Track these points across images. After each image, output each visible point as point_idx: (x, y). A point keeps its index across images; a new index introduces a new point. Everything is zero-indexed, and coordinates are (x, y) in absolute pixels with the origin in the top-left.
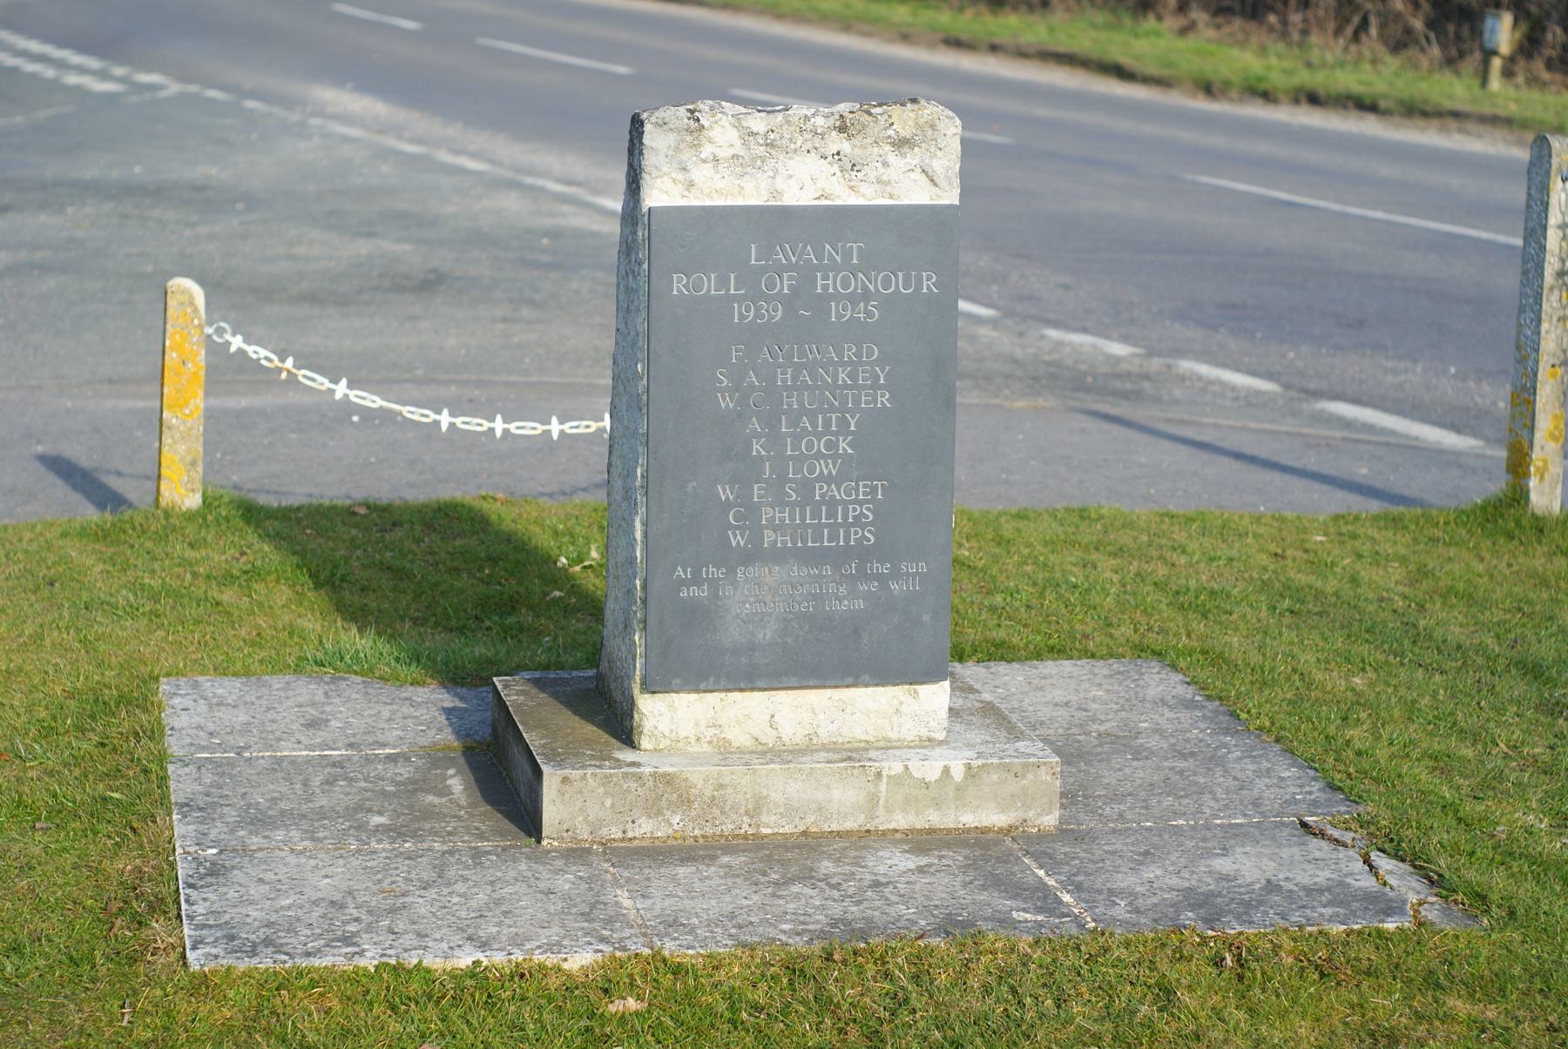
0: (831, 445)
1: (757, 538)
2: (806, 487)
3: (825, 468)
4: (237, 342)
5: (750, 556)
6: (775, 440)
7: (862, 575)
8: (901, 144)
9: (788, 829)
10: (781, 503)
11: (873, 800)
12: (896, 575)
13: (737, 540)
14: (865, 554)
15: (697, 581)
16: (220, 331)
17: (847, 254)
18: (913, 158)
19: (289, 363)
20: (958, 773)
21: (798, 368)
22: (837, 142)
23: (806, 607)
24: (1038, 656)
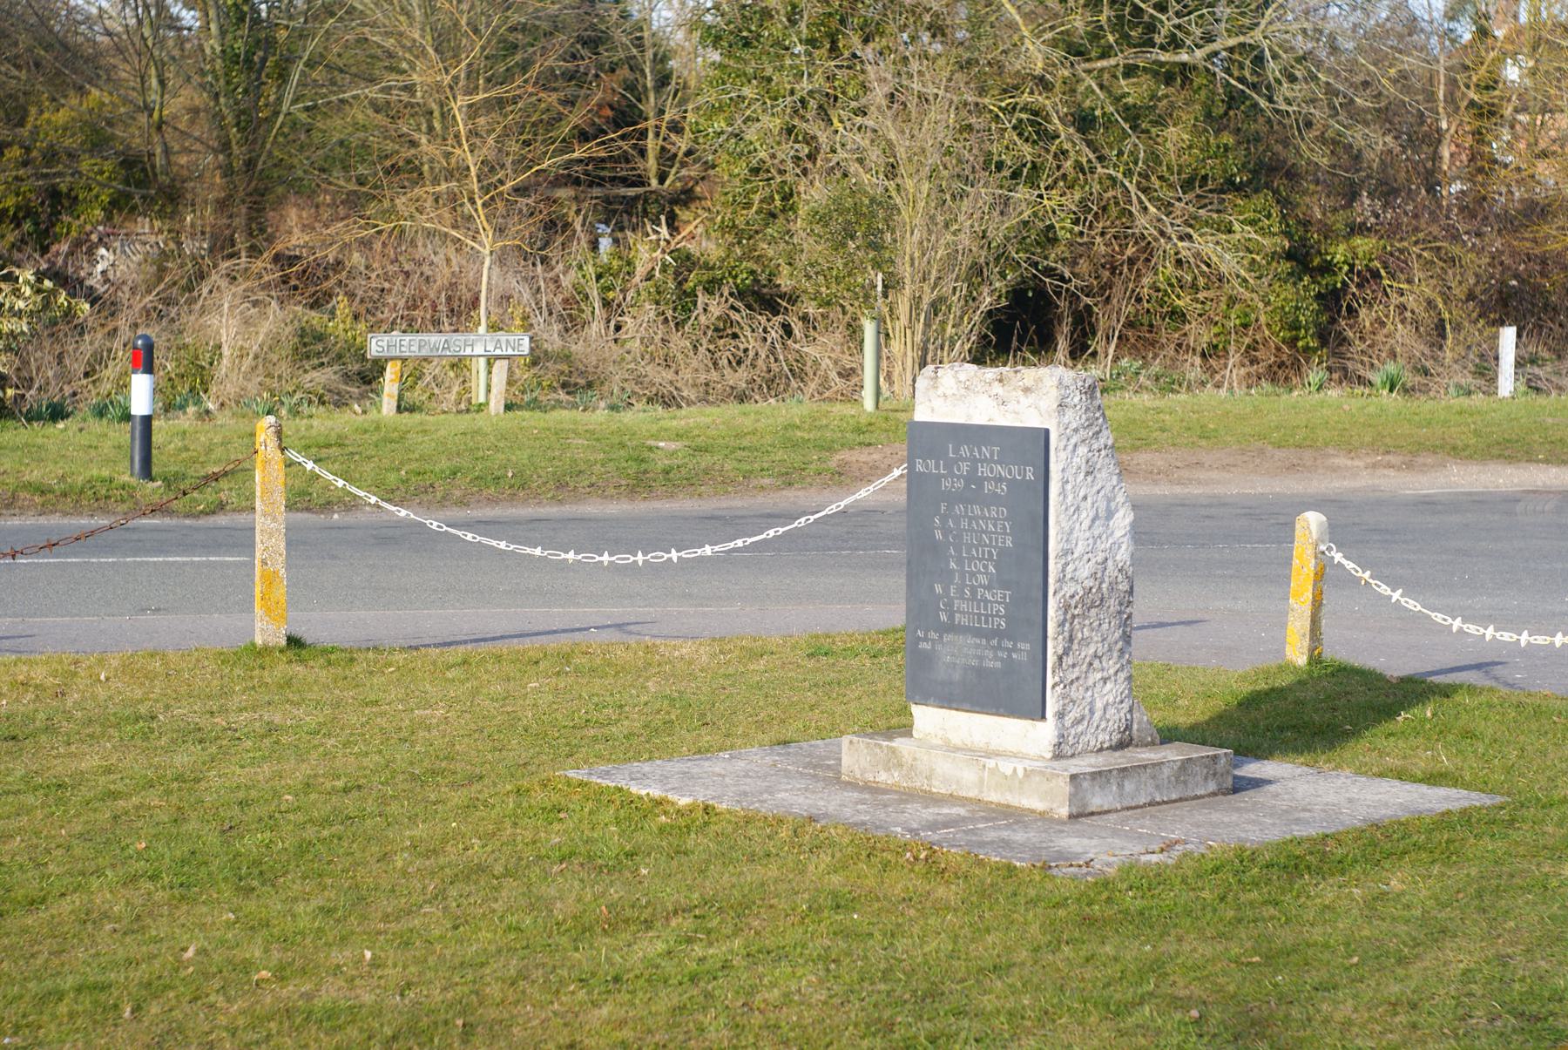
0: (985, 567)
1: (951, 617)
2: (973, 590)
3: (983, 579)
4: (1338, 557)
5: (951, 628)
6: (960, 561)
7: (999, 647)
8: (1027, 390)
9: (943, 791)
10: (962, 598)
11: (981, 781)
12: (1015, 649)
13: (943, 617)
14: (997, 633)
15: (926, 639)
16: (1329, 549)
17: (992, 455)
18: (1032, 398)
19: (1367, 575)
20: (1020, 773)
21: (970, 519)
22: (997, 388)
23: (975, 662)
24: (1381, 775)
